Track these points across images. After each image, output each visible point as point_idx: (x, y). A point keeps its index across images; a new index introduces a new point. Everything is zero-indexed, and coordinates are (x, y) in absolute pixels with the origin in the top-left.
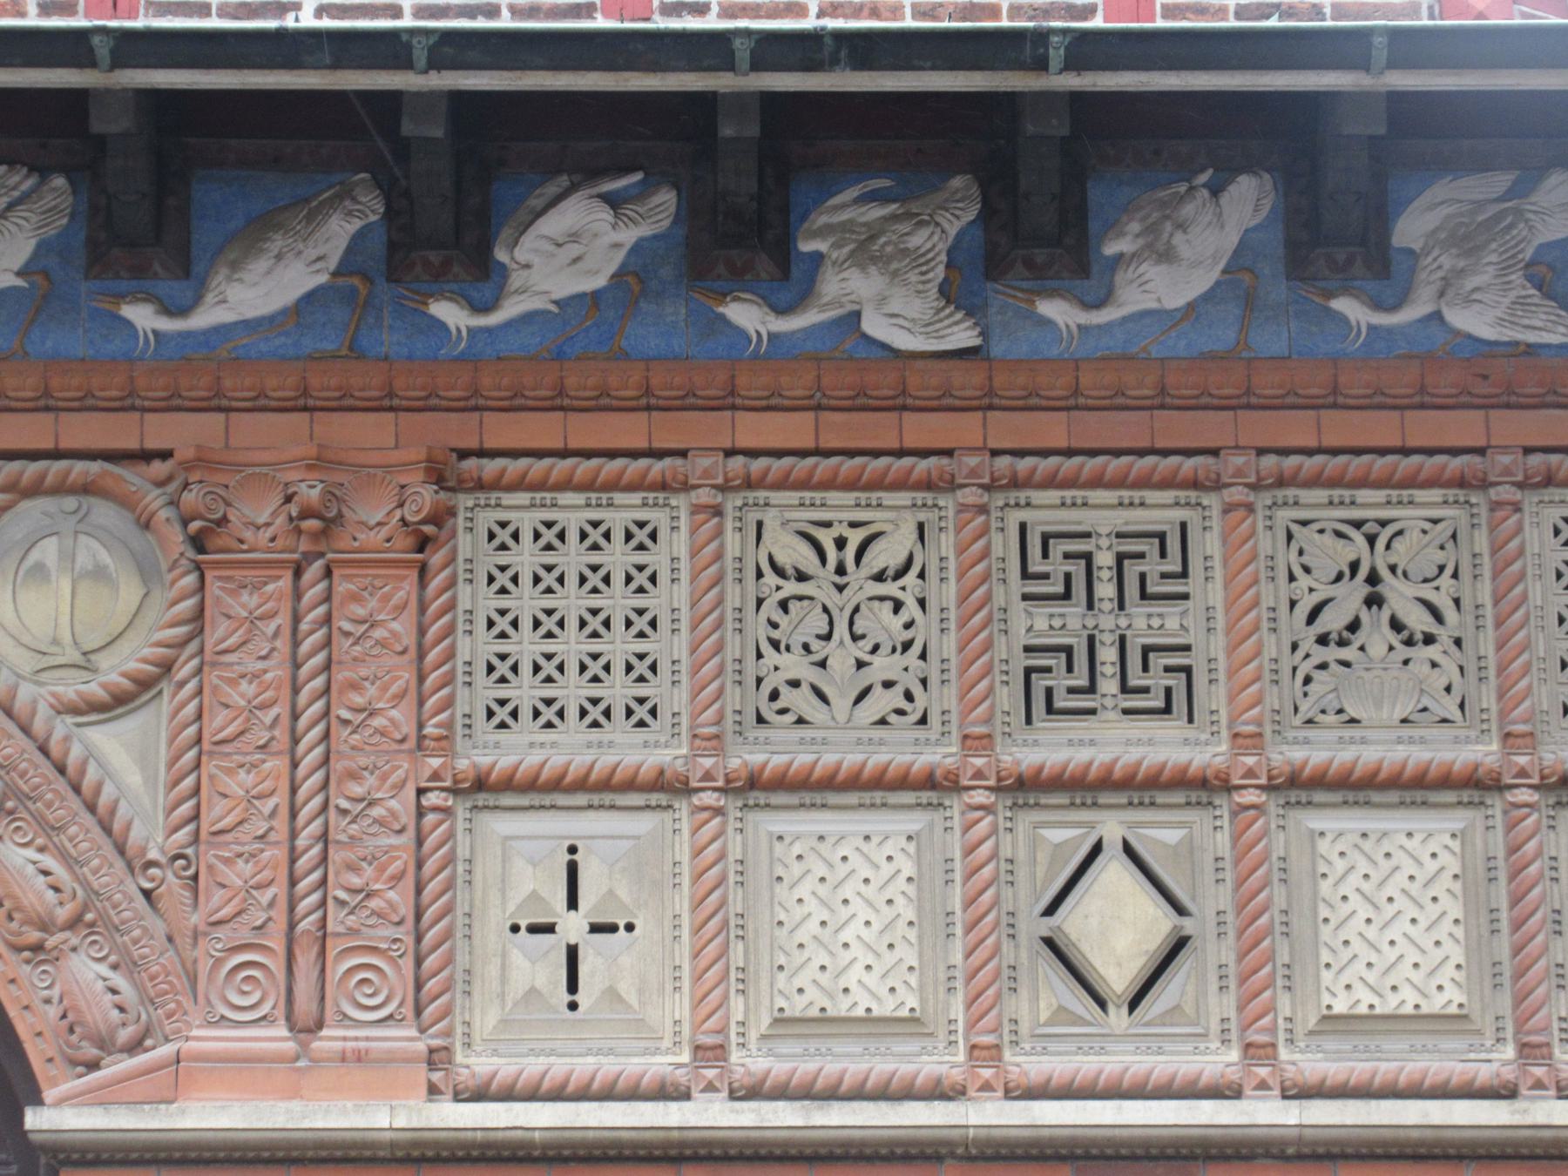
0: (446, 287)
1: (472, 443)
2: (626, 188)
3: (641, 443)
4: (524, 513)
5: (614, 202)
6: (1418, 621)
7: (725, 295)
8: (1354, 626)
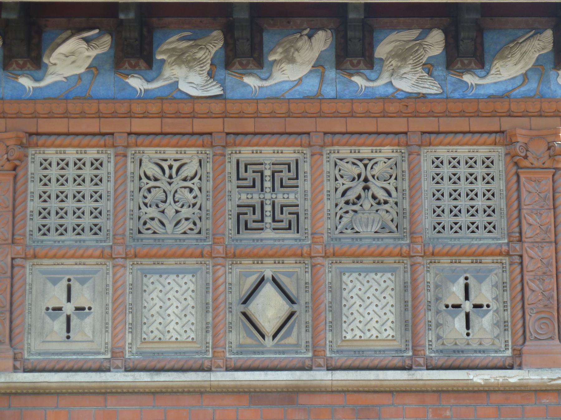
0: (25, 72)
1: (33, 130)
2: (92, 35)
3: (96, 130)
4: (52, 154)
5: (87, 40)
7: (128, 75)
8: (359, 198)
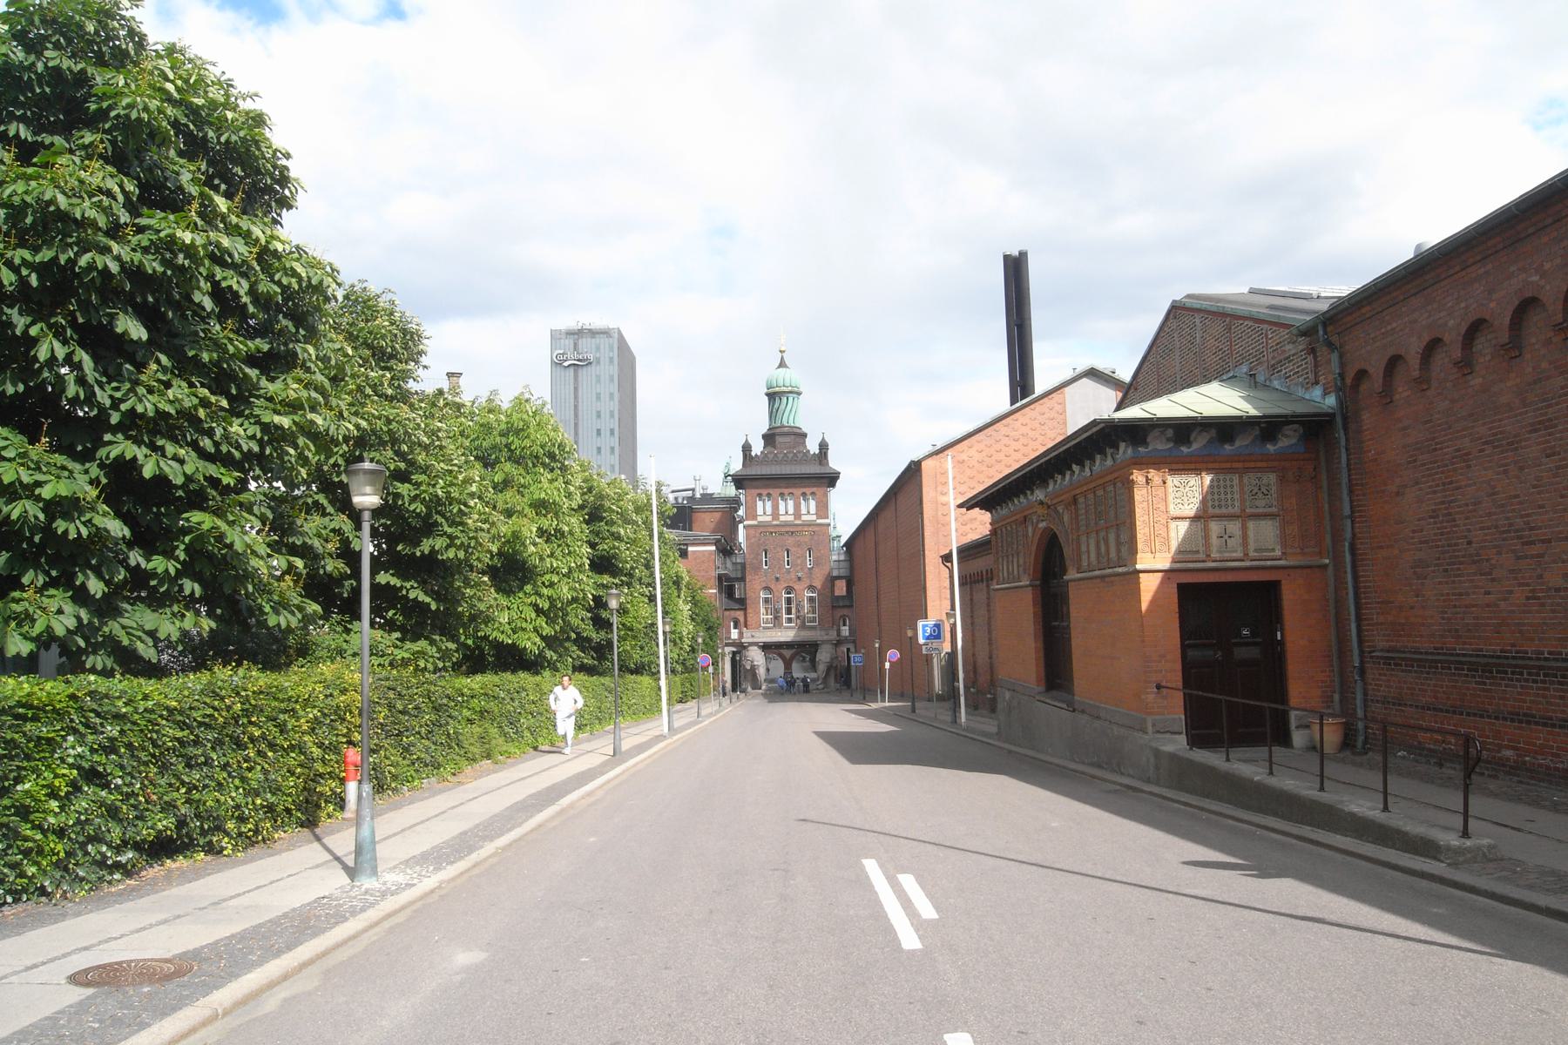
6: (1266, 492)
